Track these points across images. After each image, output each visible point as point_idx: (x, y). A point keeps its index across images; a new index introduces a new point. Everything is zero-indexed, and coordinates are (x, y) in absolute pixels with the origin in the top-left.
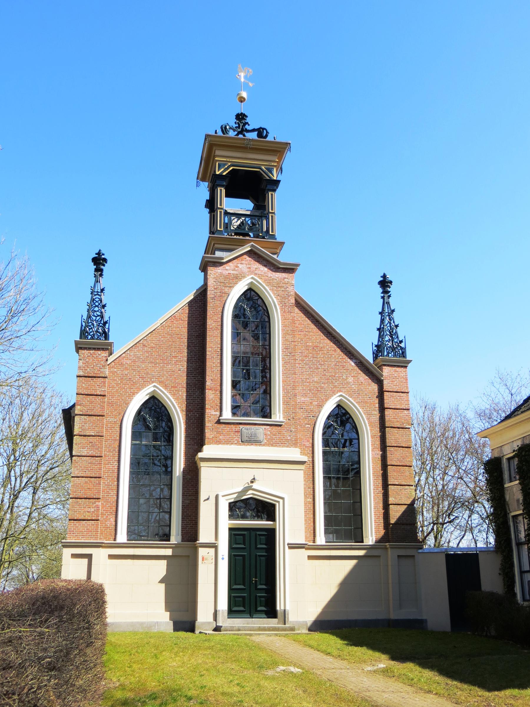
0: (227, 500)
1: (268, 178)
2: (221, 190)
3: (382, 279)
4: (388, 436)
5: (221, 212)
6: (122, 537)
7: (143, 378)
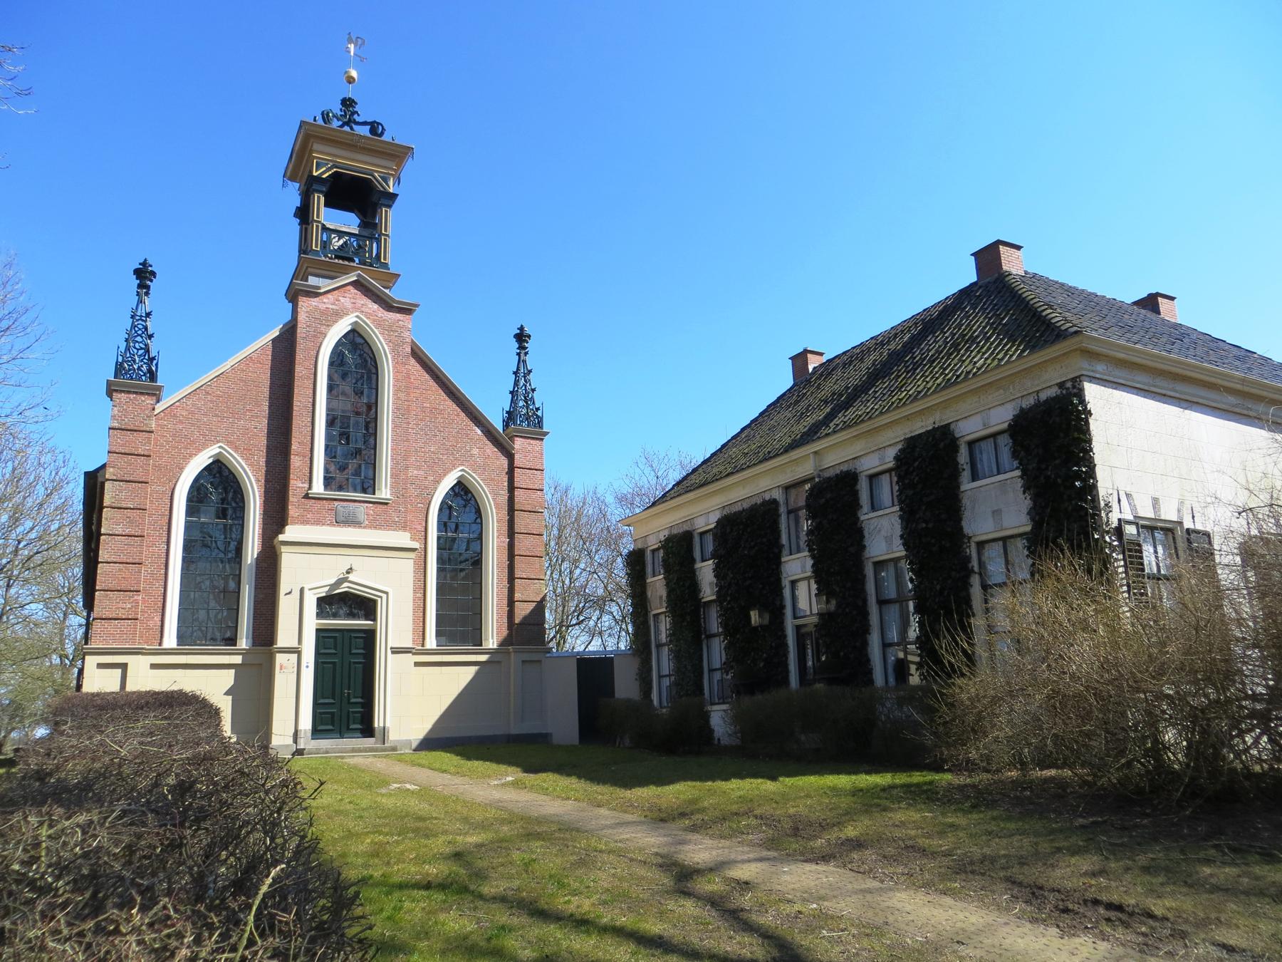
1: (382, 189)
2: (319, 197)
3: (518, 331)
5: (317, 226)
6: (170, 640)
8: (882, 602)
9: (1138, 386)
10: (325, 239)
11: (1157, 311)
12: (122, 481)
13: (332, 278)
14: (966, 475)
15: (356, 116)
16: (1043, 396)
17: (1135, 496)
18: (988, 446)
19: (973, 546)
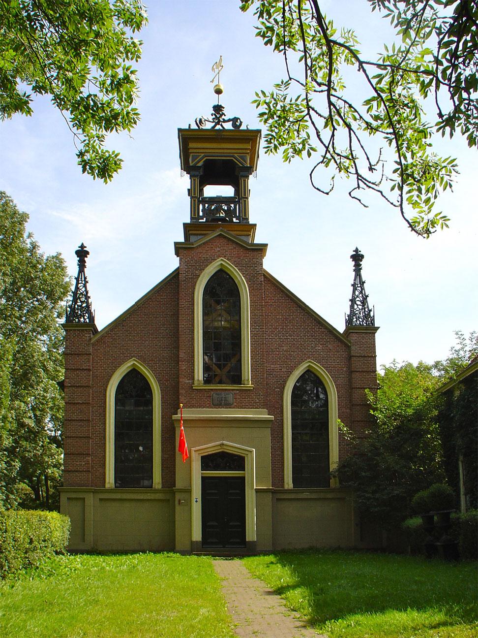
1: (241, 166)
3: (354, 253)
7: (123, 353)
13: (205, 235)
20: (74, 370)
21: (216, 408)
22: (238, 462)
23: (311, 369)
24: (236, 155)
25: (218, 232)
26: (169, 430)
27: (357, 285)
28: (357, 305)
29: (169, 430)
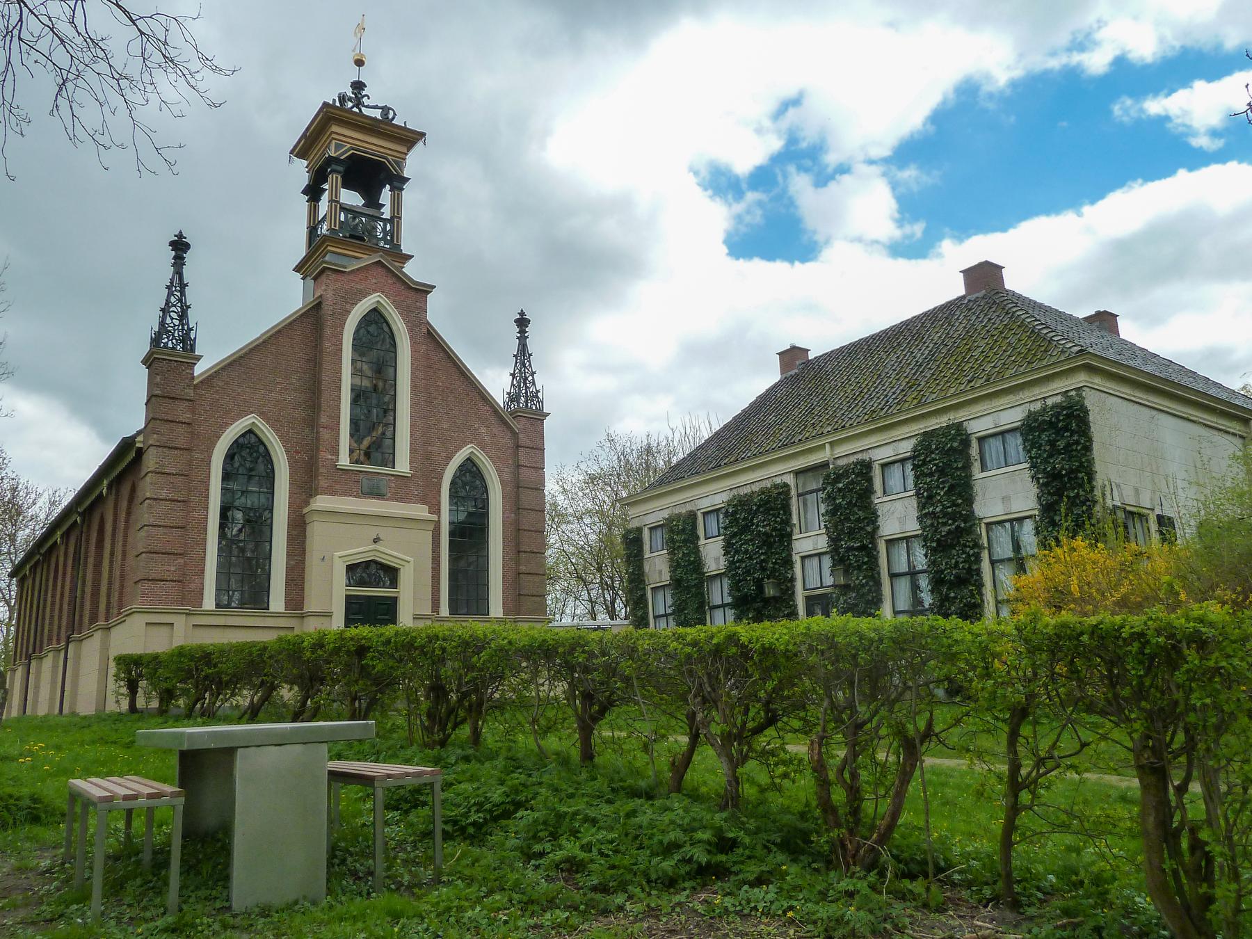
0: (344, 562)
2: (337, 178)
4: (522, 496)
5: (336, 206)
6: (209, 603)
8: (893, 576)
9: (1123, 395)
10: (342, 219)
11: (1114, 330)
12: (165, 447)
14: (976, 466)
15: (365, 99)
16: (1050, 402)
17: (1122, 486)
18: (995, 446)
19: (983, 526)
20: (166, 421)
21: (365, 498)
22: (390, 574)
23: (474, 458)
24: (389, 157)
25: (375, 258)
26: (299, 527)
27: (176, 287)
28: (172, 319)
29: (299, 527)
